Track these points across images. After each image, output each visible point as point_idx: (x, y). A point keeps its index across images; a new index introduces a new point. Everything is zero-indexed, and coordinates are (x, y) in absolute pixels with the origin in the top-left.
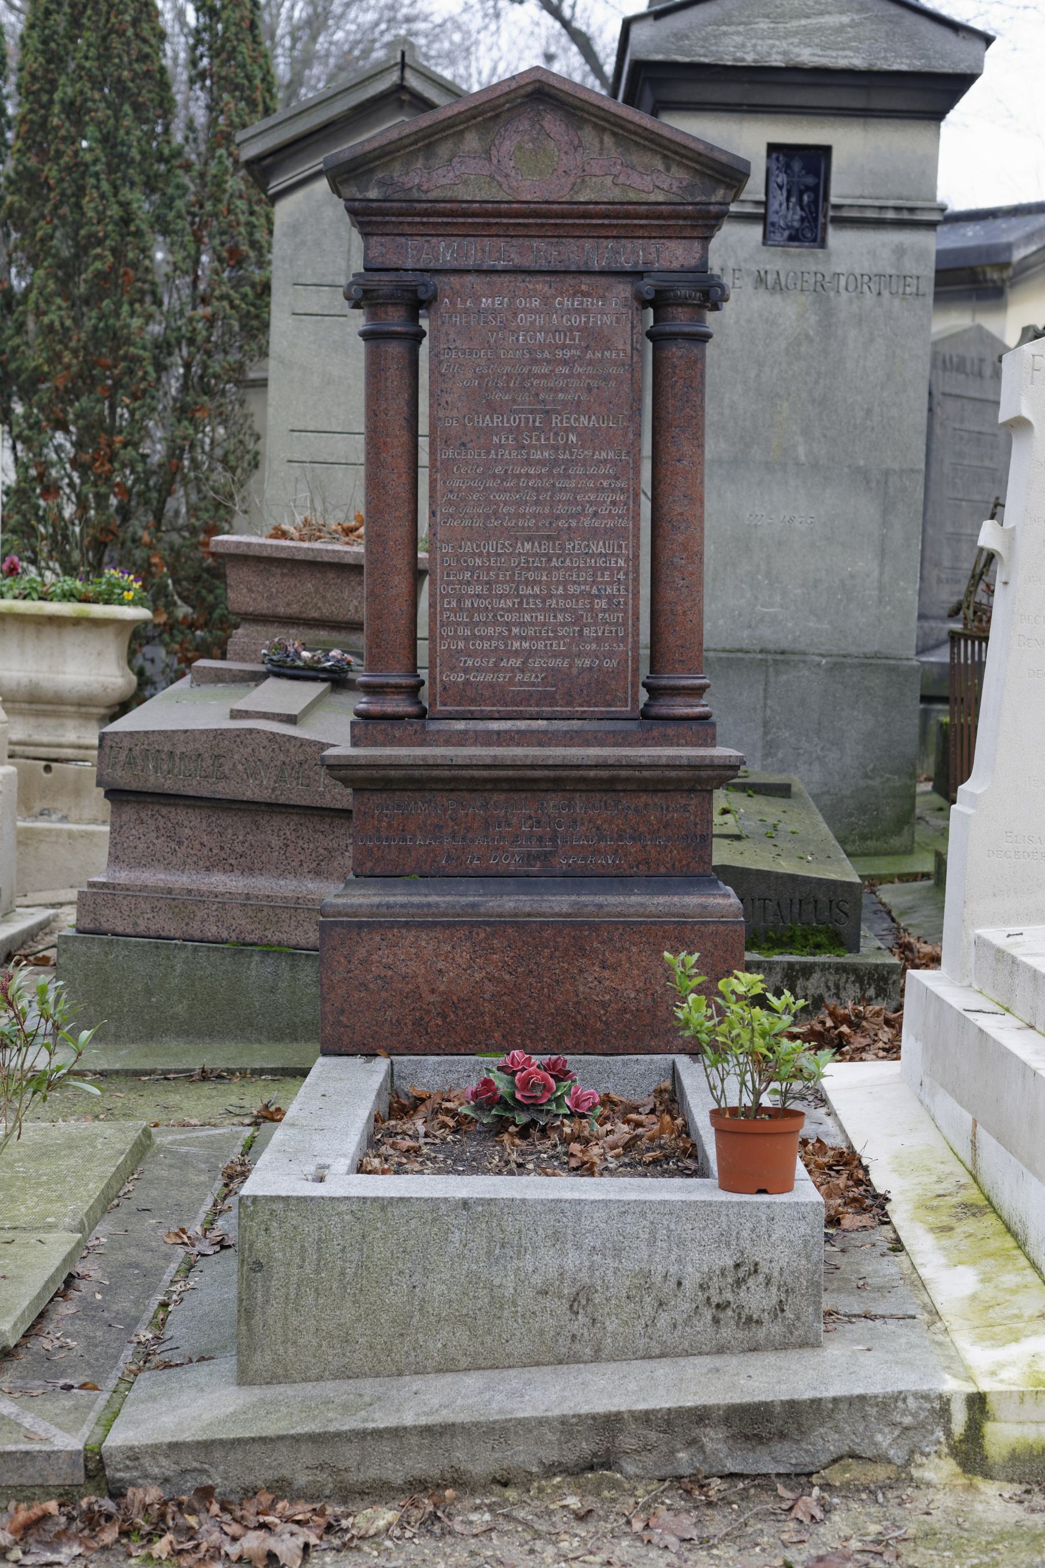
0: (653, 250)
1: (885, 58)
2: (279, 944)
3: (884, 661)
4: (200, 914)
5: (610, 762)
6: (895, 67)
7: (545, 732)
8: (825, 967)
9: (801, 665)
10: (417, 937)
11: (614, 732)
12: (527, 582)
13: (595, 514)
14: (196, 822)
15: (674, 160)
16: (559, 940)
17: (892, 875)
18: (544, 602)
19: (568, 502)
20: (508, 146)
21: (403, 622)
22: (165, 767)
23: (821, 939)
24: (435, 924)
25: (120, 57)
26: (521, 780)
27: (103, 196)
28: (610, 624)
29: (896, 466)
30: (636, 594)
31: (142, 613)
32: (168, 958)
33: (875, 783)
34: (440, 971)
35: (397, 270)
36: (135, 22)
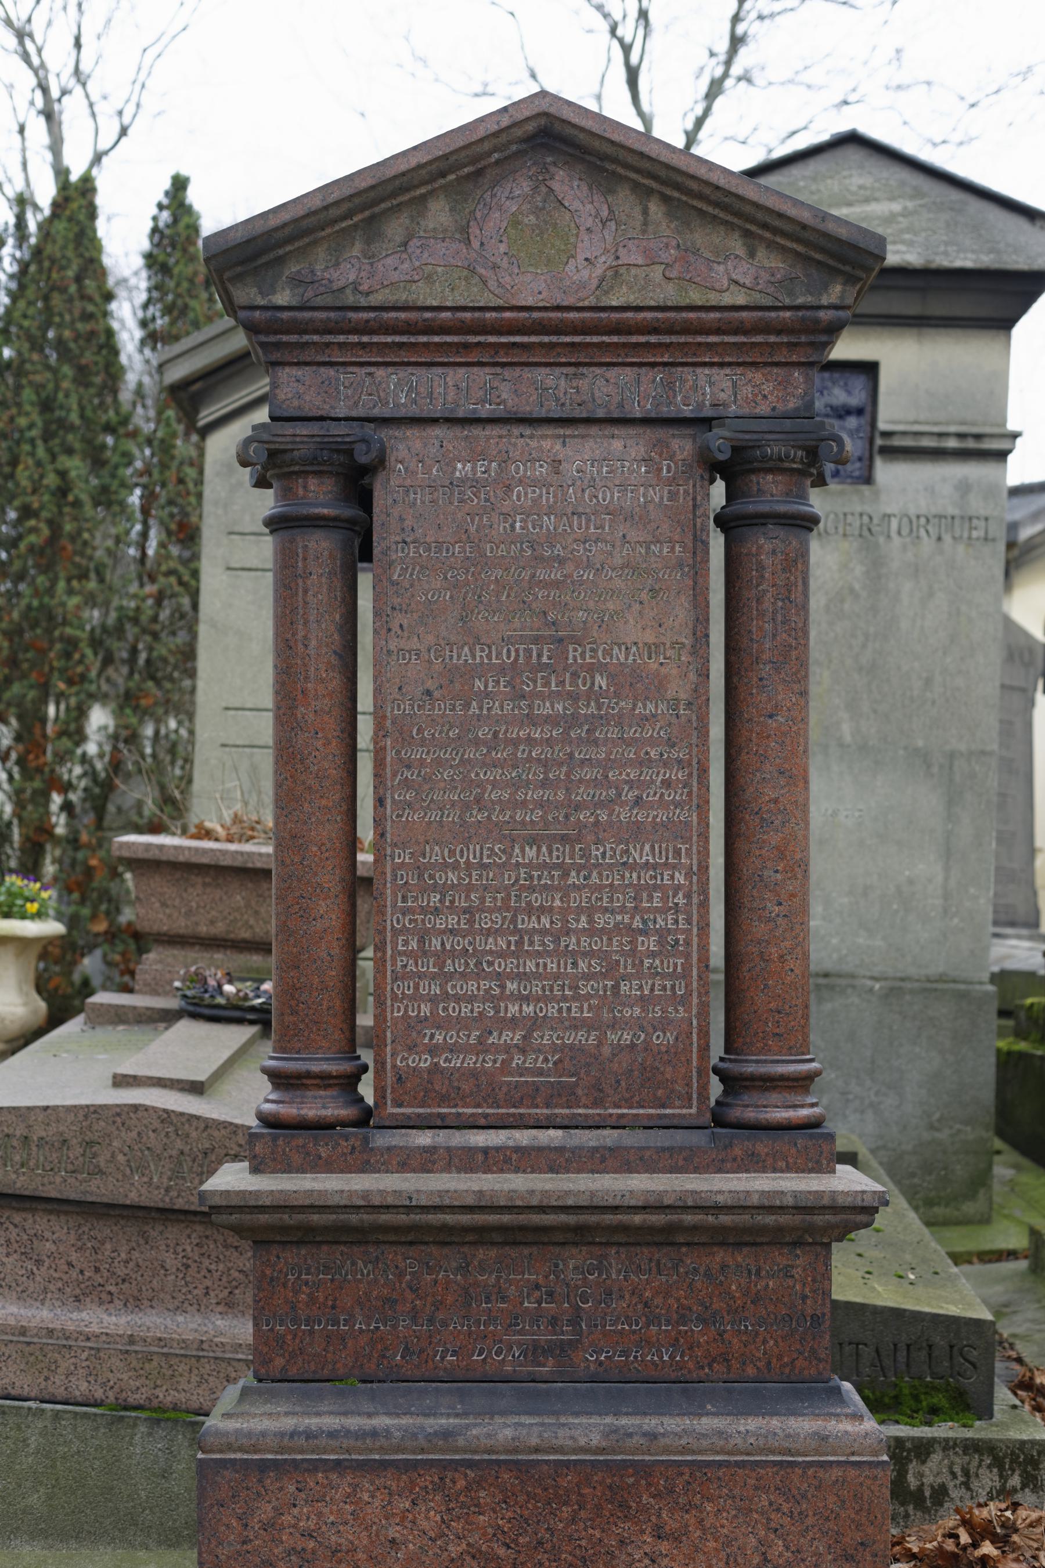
0: (727, 384)
1: (946, 253)
2: (175, 1408)
3: (952, 986)
4: (65, 1365)
5: (667, 1201)
6: (958, 264)
7: (560, 1150)
8: (948, 1445)
9: (849, 991)
10: (355, 1487)
11: (670, 1149)
12: (530, 910)
13: (638, 801)
14: (61, 1234)
15: (761, 238)
16: (586, 1491)
17: (970, 1254)
18: (557, 941)
19: (595, 783)
20: (496, 221)
21: (334, 974)
22: (17, 1158)
23: (939, 1400)
24: (384, 1465)
25: (61, 315)
26: (522, 1228)
27: (39, 464)
28: (663, 976)
29: (963, 747)
30: (704, 928)
31: (53, 927)
32: (19, 1428)
33: (943, 1135)
34: (393, 1541)
35: (322, 419)
36: (78, 279)
